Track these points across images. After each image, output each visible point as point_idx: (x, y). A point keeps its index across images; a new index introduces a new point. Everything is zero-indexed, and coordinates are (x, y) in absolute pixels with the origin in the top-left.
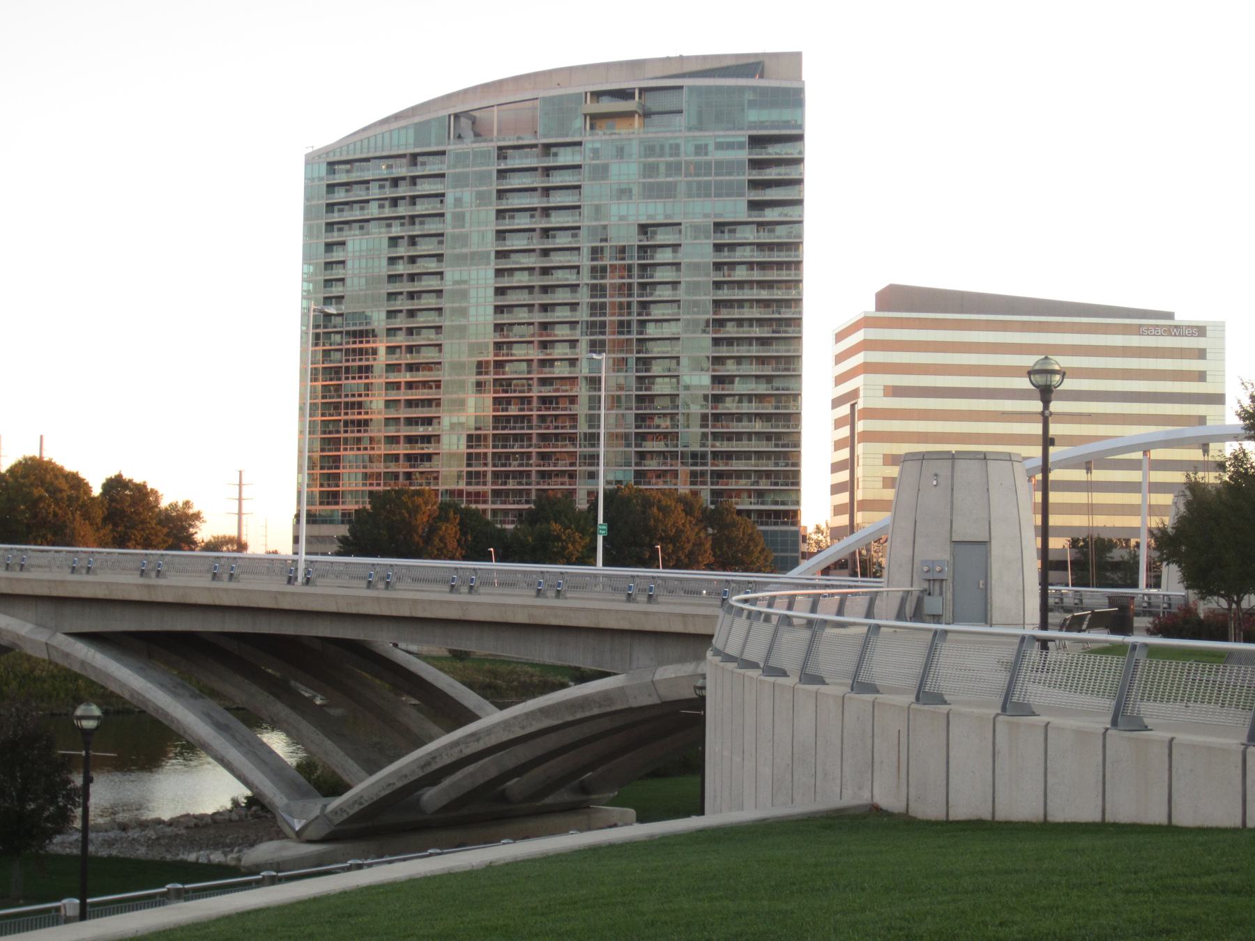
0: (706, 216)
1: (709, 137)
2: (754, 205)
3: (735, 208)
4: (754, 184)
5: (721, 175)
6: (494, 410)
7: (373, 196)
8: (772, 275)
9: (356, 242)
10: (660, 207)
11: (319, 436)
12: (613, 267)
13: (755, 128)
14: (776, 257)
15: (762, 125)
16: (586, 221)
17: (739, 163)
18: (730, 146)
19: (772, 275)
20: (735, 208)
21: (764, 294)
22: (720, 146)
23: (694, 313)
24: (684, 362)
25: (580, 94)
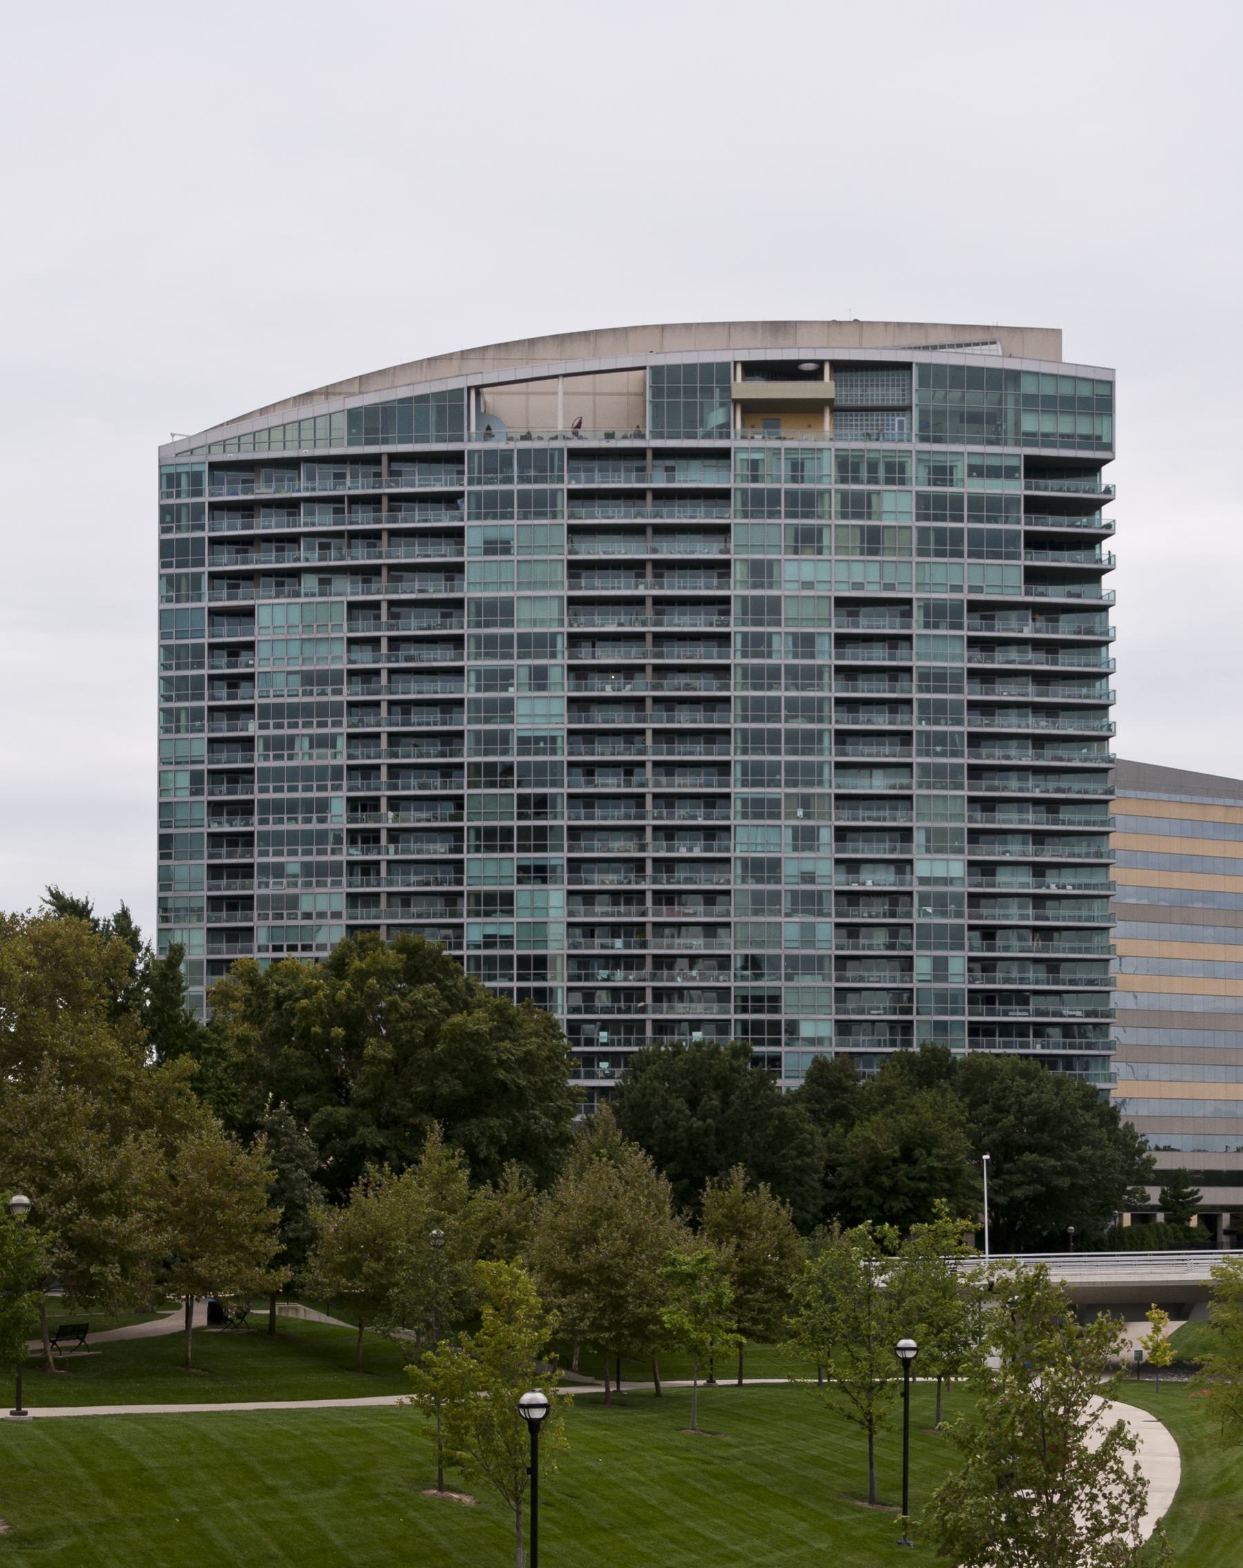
0: (958, 588)
1: (962, 451)
2: (1034, 576)
3: (1004, 579)
4: (1036, 542)
5: (979, 520)
6: (210, 952)
7: (284, 531)
8: (1059, 695)
9: (274, 614)
10: (873, 573)
11: (664, 908)
12: (791, 670)
13: (1035, 444)
14: (1066, 663)
15: (1046, 439)
16: (737, 589)
17: (1012, 501)
18: (994, 472)
19: (1059, 695)
20: (1004, 579)
21: (1042, 727)
22: (976, 471)
23: (937, 754)
24: (919, 838)
25: (728, 364)
